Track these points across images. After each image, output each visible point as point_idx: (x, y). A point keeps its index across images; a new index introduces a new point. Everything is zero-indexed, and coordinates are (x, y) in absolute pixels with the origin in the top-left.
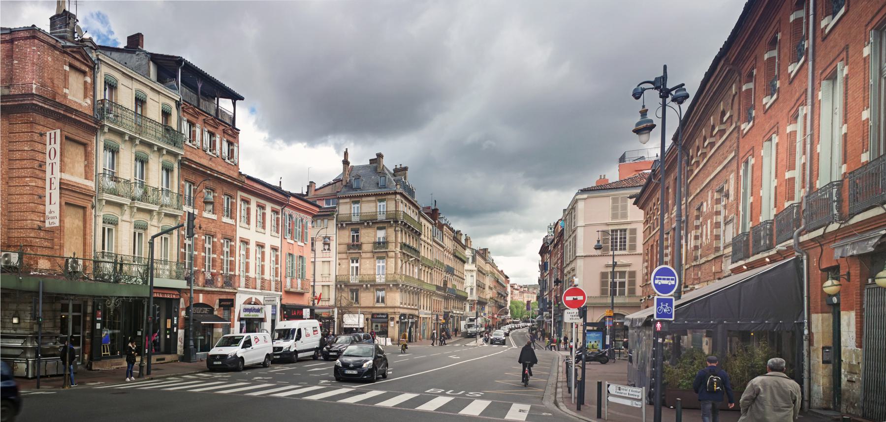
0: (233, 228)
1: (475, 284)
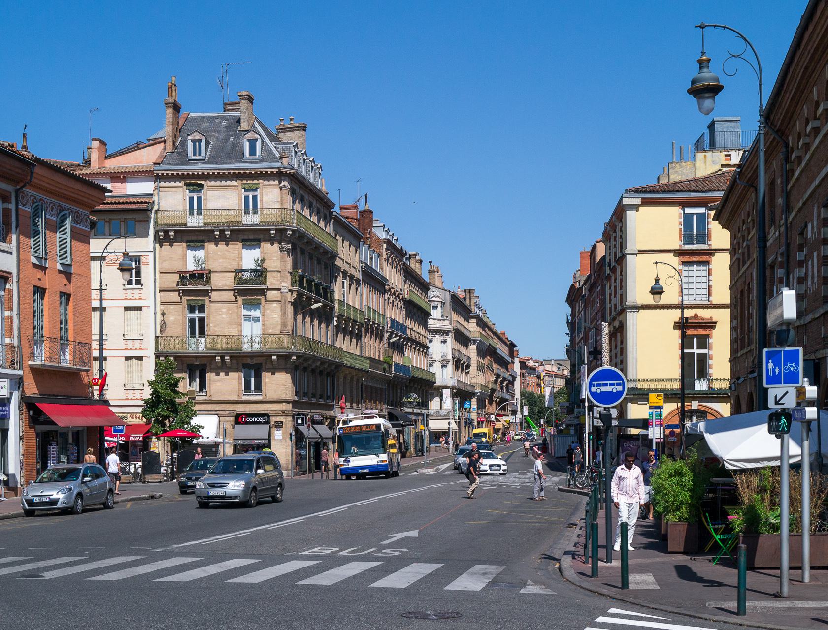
1: (450, 357)
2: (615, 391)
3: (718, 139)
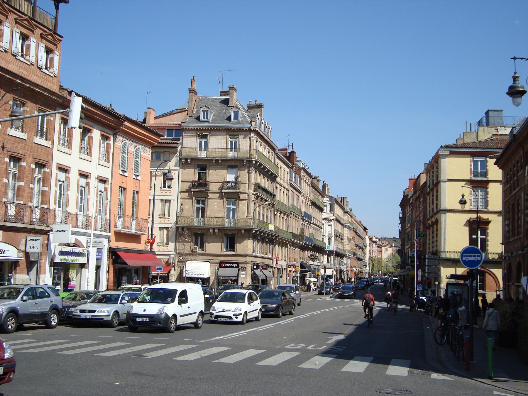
0: (49, 151)
1: (333, 234)
2: (476, 260)
3: (491, 120)
